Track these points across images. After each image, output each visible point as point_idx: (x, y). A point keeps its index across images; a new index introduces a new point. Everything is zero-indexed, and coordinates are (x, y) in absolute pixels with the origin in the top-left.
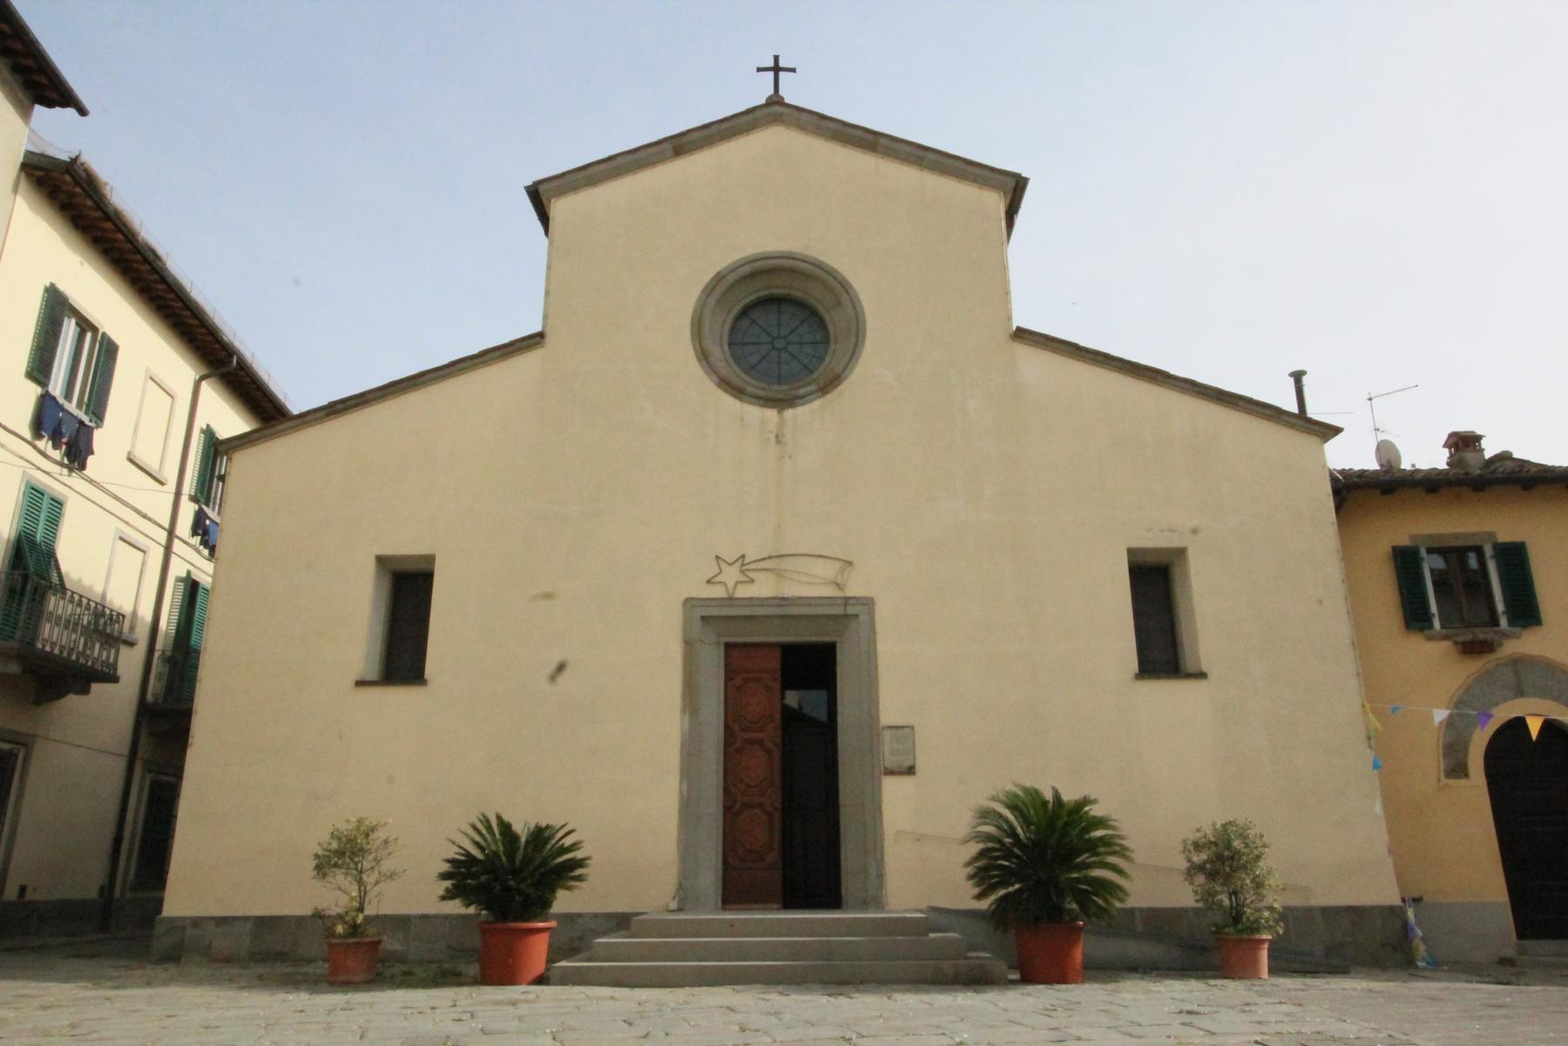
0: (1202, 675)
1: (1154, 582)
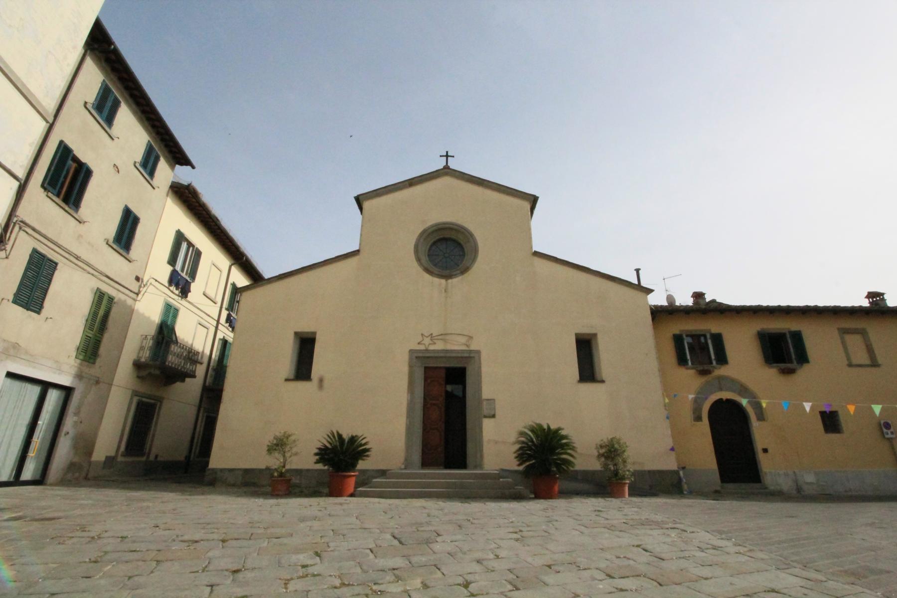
0: (603, 381)
1: (585, 347)
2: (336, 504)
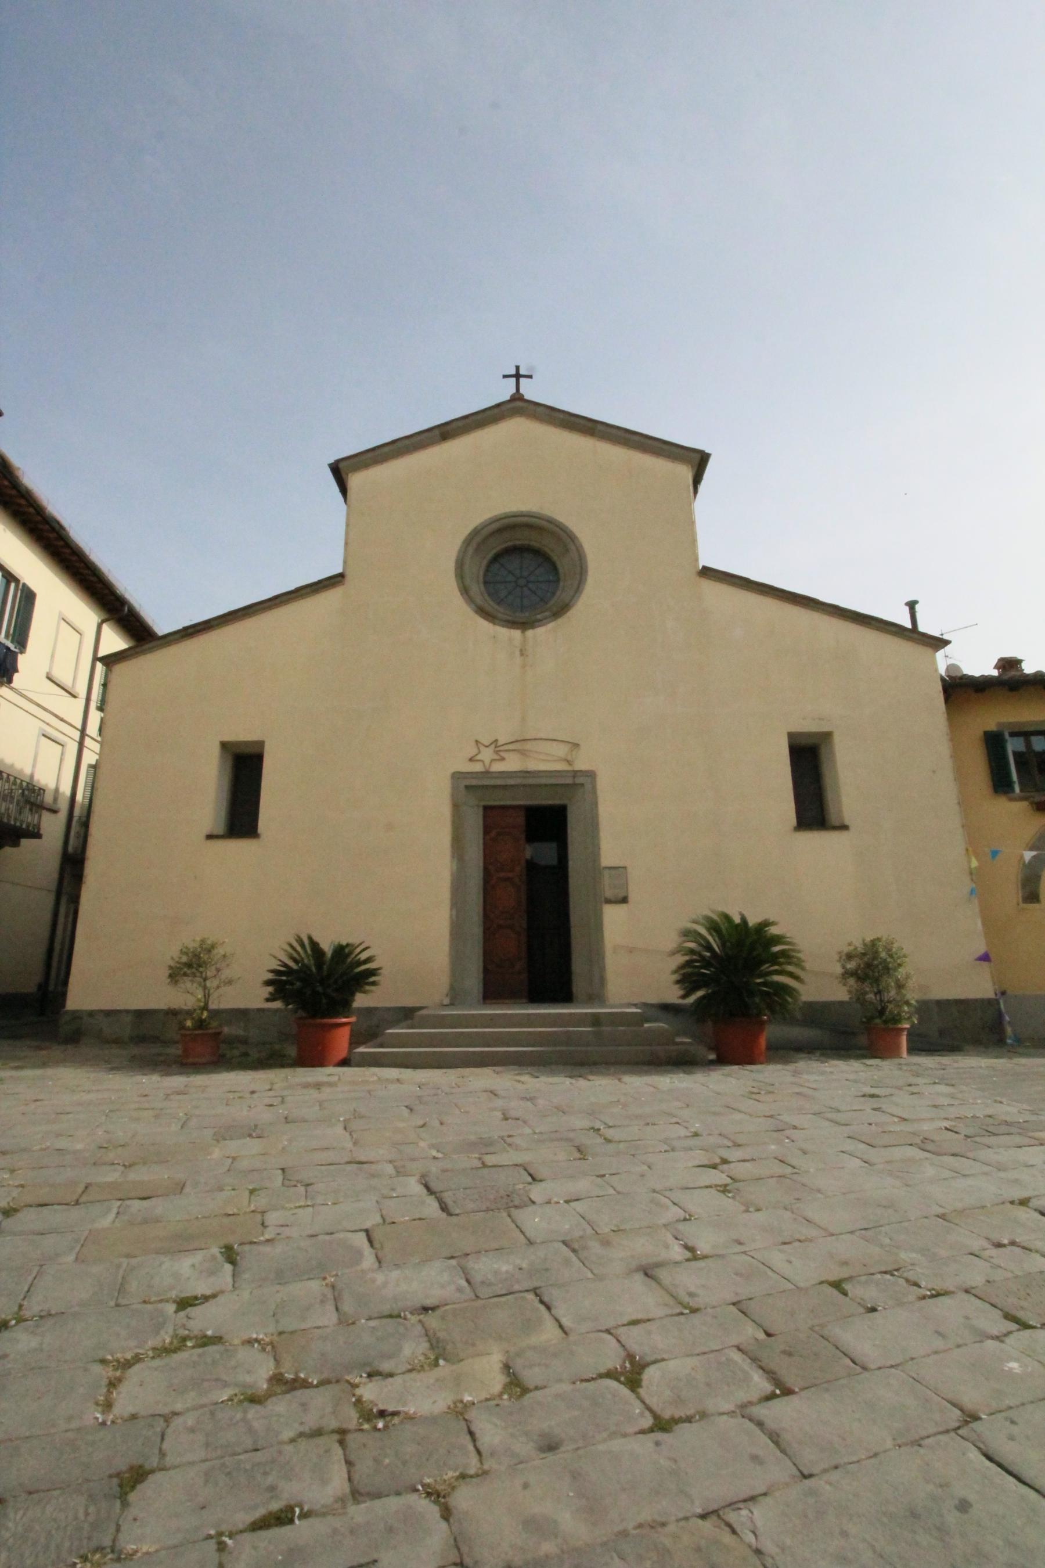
0: (844, 827)
1: (808, 758)
2: (306, 1086)
